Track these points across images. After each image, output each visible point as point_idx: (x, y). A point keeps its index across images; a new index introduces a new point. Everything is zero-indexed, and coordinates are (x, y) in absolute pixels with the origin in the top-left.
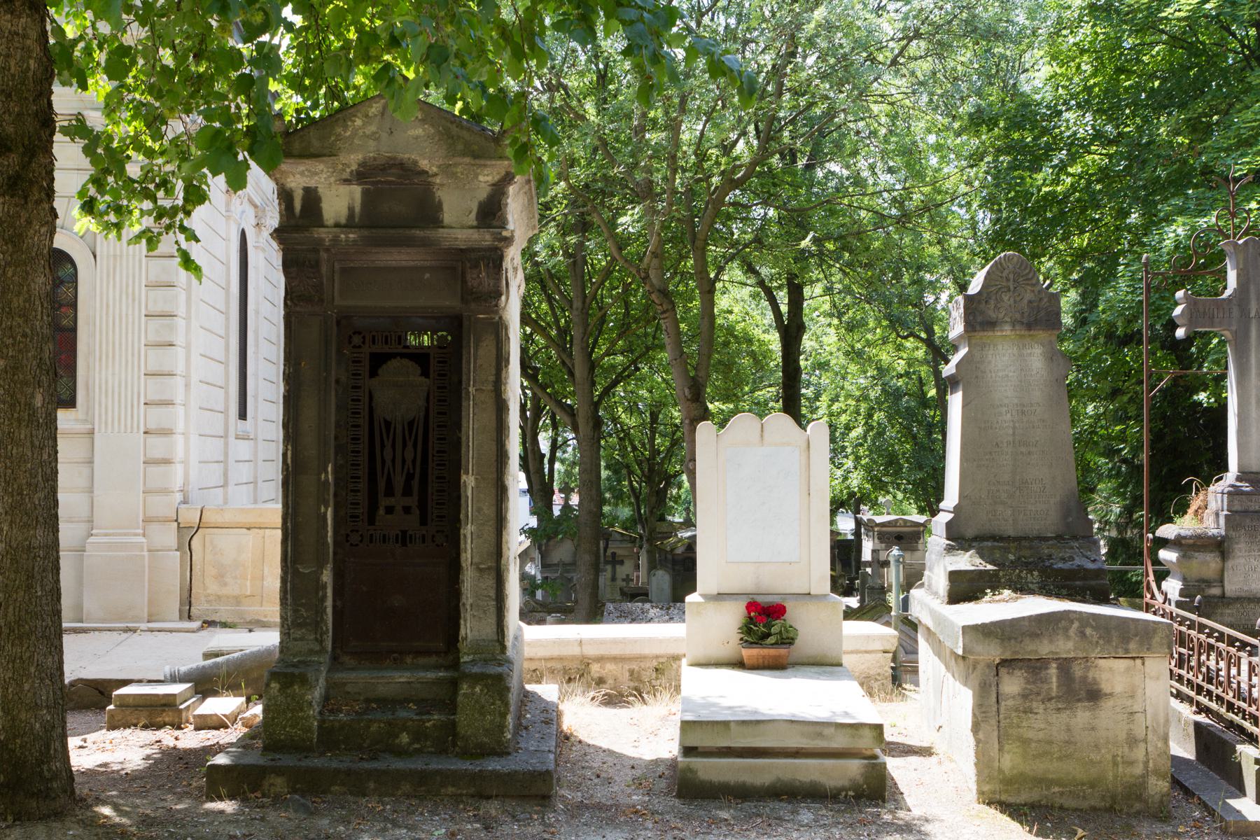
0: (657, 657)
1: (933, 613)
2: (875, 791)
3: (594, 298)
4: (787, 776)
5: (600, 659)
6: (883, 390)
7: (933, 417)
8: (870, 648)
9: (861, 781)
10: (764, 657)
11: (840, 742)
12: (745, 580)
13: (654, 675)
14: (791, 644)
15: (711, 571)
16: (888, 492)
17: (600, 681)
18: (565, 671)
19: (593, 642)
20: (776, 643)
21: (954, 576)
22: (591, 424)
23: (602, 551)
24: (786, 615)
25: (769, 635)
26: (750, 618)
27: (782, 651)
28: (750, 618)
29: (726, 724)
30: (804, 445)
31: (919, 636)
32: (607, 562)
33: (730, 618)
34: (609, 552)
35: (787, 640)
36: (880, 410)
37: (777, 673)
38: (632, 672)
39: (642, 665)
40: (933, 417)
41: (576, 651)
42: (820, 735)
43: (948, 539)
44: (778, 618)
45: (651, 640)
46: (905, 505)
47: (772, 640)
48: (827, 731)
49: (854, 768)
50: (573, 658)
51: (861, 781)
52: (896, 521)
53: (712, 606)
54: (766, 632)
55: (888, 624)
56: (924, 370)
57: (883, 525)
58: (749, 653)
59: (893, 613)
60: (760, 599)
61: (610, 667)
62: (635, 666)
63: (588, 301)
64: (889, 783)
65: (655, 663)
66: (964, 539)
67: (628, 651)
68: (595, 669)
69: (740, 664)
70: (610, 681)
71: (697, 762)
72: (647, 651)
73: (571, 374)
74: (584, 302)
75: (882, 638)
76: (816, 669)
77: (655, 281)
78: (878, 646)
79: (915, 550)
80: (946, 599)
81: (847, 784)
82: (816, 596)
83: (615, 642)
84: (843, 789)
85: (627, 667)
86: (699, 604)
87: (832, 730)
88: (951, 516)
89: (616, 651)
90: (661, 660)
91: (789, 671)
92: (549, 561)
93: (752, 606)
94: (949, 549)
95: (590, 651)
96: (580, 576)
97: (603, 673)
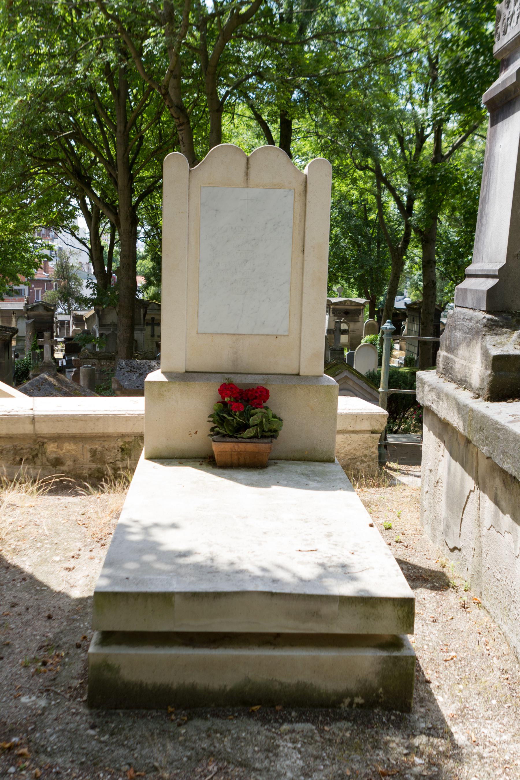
0: (123, 436)
1: (461, 409)
2: (396, 697)
3: (134, 123)
4: (261, 676)
5: (57, 438)
6: (340, 213)
7: (372, 234)
8: (358, 428)
9: (375, 682)
10: (239, 453)
11: (346, 624)
12: (217, 355)
13: (119, 456)
14: (274, 437)
15: (181, 339)
16: (338, 283)
17: (57, 462)
18: (16, 451)
19: (48, 419)
20: (255, 437)
21: (500, 364)
22: (129, 221)
23: (142, 316)
24: (267, 404)
25: (246, 426)
26: (225, 404)
27: (263, 446)
28: (225, 404)
29: (166, 597)
30: (300, 188)
31: (424, 425)
32: (147, 324)
33: (192, 411)
34: (148, 317)
35: (269, 433)
36: (337, 226)
37: (254, 475)
38: (94, 452)
39: (106, 445)
40: (372, 234)
41: (28, 429)
42: (316, 615)
43: (488, 312)
44: (259, 406)
45: (116, 418)
46: (349, 292)
47: (250, 432)
48: (326, 609)
49: (366, 662)
50: (24, 437)
51: (375, 682)
52: (346, 301)
53: (177, 389)
54: (245, 430)
55: (373, 400)
56: (371, 198)
57: (336, 304)
58: (219, 448)
59: (380, 390)
60: (237, 380)
61: (69, 447)
62: (97, 446)
63: (128, 125)
64: (419, 692)
65: (120, 443)
66: (510, 313)
67: (89, 429)
68: (51, 448)
69: (209, 461)
70: (69, 463)
71: (121, 654)
72: (110, 430)
73: (116, 183)
74: (125, 127)
75: (371, 417)
76: (301, 467)
77: (173, 98)
78: (366, 426)
79: (356, 321)
80: (486, 393)
81: (353, 686)
82: (307, 377)
83: (74, 419)
84: (348, 694)
85: (88, 447)
86: (161, 384)
87: (335, 607)
88: (496, 280)
89: (74, 429)
90: (127, 440)
91: (270, 473)
92: (104, 322)
93: (226, 389)
94: (491, 327)
95: (44, 429)
96: (122, 334)
97: (61, 453)
